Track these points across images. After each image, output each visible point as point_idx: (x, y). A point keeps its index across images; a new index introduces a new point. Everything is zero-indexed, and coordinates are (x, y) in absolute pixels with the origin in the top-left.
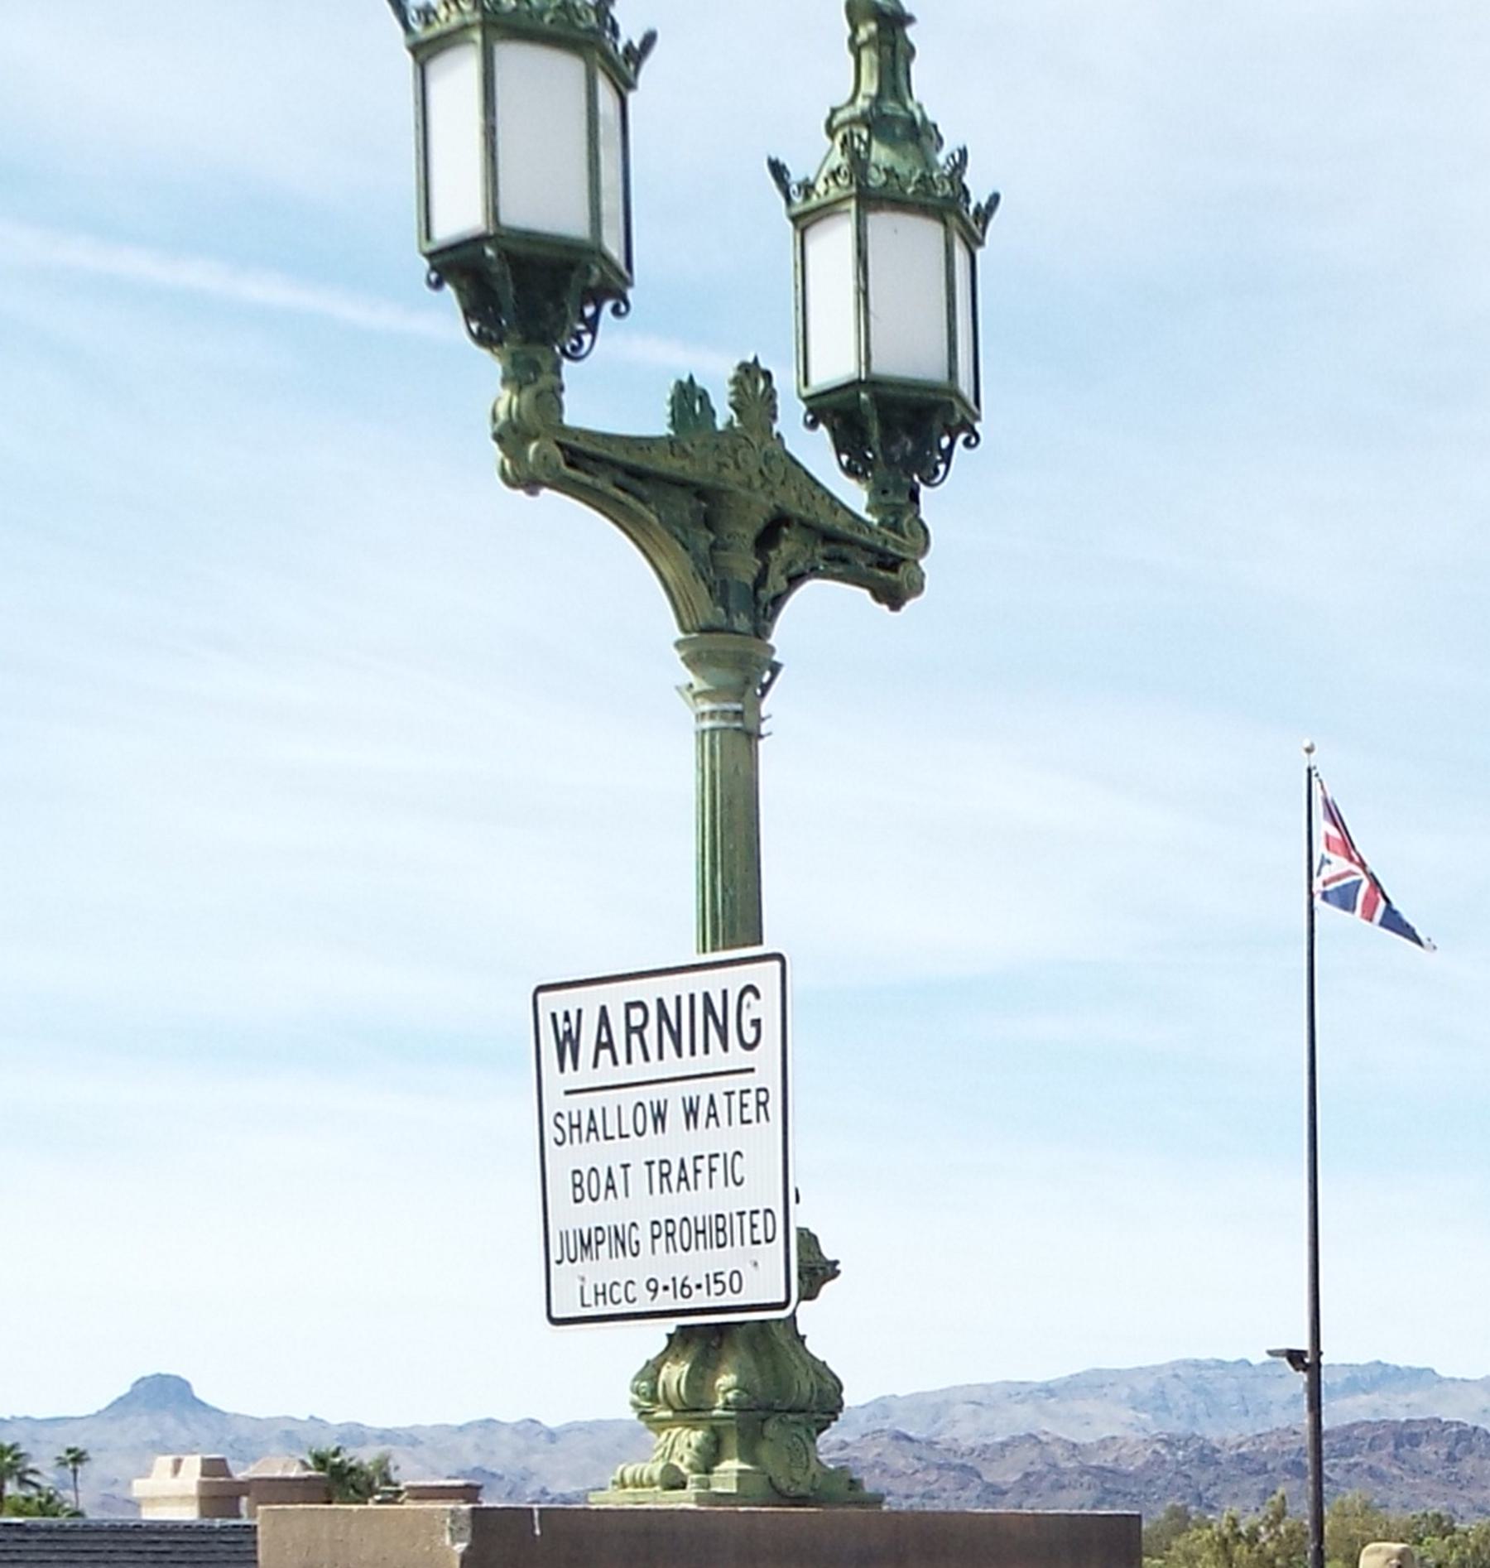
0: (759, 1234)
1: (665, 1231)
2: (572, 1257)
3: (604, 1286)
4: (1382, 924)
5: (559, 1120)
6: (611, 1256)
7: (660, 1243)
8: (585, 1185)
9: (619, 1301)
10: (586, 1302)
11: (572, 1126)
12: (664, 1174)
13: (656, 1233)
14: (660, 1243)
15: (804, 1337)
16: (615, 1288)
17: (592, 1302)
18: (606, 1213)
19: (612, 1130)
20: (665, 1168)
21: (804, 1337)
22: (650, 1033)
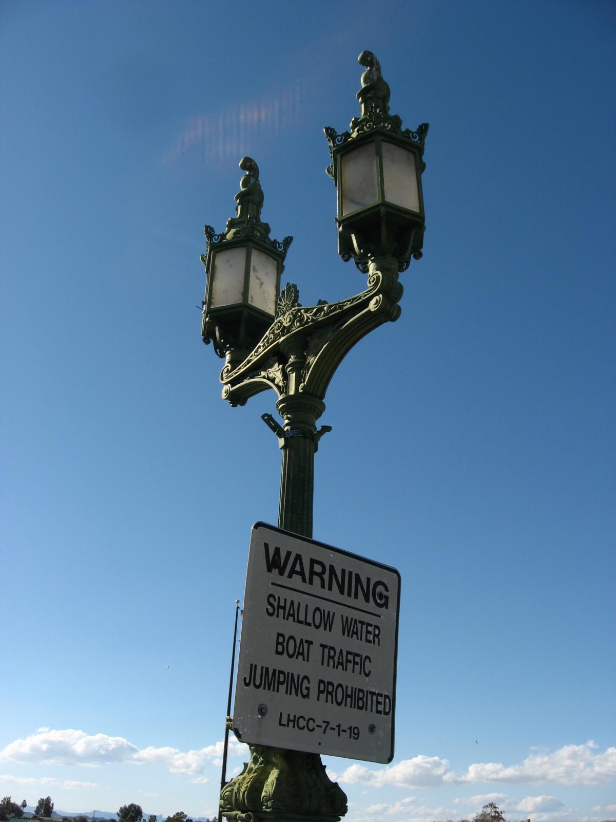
0: (381, 708)
1: (327, 689)
2: (257, 683)
3: (295, 716)
4: (297, 622)
5: (271, 600)
6: (287, 693)
7: (323, 696)
8: (285, 644)
9: (304, 728)
10: (282, 723)
11: (279, 607)
12: (331, 656)
13: (322, 688)
14: (323, 696)
15: (325, 766)
16: (301, 720)
17: (286, 723)
18: (295, 667)
19: (302, 618)
20: (332, 653)
21: (325, 766)
22: (326, 577)
